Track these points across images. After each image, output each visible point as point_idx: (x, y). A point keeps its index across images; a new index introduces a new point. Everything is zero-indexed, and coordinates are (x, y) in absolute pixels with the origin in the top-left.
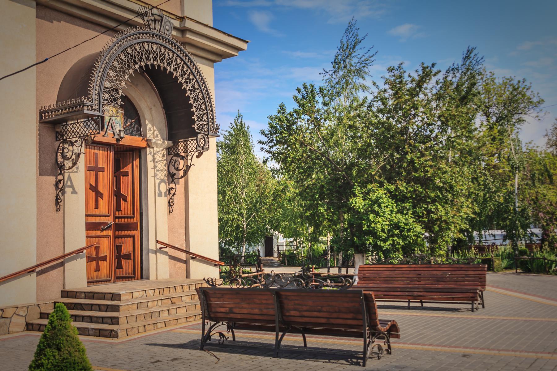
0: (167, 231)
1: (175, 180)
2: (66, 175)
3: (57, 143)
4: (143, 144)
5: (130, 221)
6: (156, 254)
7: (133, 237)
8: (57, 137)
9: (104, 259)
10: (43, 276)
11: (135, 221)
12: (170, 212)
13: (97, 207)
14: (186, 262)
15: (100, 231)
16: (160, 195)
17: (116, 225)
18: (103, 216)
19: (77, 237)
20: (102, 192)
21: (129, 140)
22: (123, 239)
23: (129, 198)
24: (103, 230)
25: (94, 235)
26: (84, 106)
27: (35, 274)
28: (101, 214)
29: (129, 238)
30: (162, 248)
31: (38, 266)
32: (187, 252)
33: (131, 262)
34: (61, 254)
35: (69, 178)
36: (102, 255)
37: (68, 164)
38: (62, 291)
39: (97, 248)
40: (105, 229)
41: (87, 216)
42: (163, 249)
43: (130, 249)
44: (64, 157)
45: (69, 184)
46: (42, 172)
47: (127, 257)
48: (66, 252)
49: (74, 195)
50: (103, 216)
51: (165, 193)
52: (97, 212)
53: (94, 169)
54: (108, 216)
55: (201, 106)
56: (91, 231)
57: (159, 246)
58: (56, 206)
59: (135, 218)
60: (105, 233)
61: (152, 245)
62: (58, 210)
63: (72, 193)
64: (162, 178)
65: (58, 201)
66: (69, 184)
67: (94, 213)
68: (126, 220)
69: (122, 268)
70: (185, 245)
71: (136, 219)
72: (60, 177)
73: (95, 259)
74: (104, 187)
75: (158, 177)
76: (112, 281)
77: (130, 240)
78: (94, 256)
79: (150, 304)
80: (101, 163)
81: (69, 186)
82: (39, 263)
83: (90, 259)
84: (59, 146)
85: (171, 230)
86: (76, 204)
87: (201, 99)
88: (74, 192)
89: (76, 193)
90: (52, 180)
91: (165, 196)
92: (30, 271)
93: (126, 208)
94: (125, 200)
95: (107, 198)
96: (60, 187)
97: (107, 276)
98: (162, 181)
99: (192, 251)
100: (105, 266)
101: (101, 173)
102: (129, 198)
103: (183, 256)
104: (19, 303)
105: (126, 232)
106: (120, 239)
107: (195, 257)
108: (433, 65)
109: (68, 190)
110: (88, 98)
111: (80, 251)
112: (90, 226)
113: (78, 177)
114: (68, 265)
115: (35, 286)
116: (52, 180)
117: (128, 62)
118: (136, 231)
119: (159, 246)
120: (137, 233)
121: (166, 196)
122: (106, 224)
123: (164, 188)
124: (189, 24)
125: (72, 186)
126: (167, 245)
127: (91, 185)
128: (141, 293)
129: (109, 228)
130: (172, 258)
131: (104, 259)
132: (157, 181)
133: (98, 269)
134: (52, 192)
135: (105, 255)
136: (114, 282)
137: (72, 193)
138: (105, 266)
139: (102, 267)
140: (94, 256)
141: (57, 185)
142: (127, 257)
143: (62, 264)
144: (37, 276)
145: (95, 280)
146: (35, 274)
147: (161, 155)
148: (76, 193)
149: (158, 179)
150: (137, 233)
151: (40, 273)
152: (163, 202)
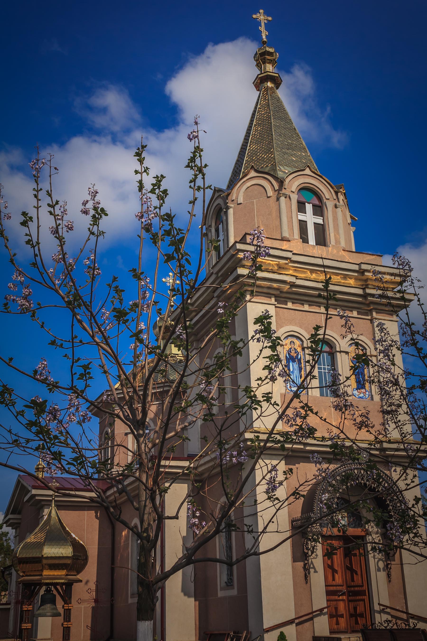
0: (388, 596)
1: (390, 558)
2: (310, 560)
3: (303, 539)
4: (363, 534)
5: (361, 589)
6: (380, 614)
7: (364, 600)
8: (303, 536)
9: (342, 616)
10: (300, 626)
11: (365, 589)
12: (390, 581)
13: (334, 579)
15: (337, 597)
16: (379, 570)
17: (349, 592)
18: (339, 586)
19: (320, 600)
20: (336, 569)
21: (352, 531)
22: (358, 602)
23: (359, 573)
24: (339, 596)
26: (311, 518)
28: (337, 584)
29: (362, 602)
30: (385, 609)
31: (296, 619)
32: (407, 613)
33: (364, 619)
34: (310, 611)
35: (312, 563)
36: (340, 613)
37: (310, 553)
38: (313, 637)
39: (336, 609)
40: (341, 595)
41: (326, 586)
42: (385, 610)
43: (363, 609)
44: (307, 549)
45: (312, 566)
46: (295, 560)
47: (361, 615)
48: (314, 610)
49: (316, 574)
50: (339, 586)
51: (383, 569)
52: (334, 583)
53: (328, 554)
54: (342, 586)
55: (396, 504)
56: (331, 597)
57: (382, 607)
58: (306, 580)
59: (364, 587)
61: (377, 607)
62: (307, 583)
64: (380, 557)
66: (312, 566)
67: (332, 584)
68: (359, 588)
69: (359, 624)
70: (405, 607)
71: (365, 587)
72: (306, 562)
73: (334, 615)
74: (338, 565)
76: (349, 632)
77: (361, 603)
78: (334, 614)
81: (312, 568)
82: (297, 617)
83: (331, 616)
84: (304, 541)
85: (391, 595)
86: (318, 579)
87: (396, 499)
88: (316, 572)
90: (302, 564)
91: (383, 571)
93: (358, 579)
94: (356, 574)
95: (340, 573)
96: (307, 569)
97: (345, 629)
98: (380, 560)
99: (410, 611)
100: (343, 622)
101: (335, 556)
102: (359, 573)
103: (404, 616)
105: (359, 597)
106: (356, 602)
109: (312, 571)
110: (313, 513)
111: (321, 610)
112: (329, 593)
113: (318, 561)
114: (315, 620)
115: (295, 632)
116: (302, 564)
117: (338, 485)
118: (365, 597)
119: (382, 607)
120: (366, 598)
121: (384, 570)
122: (340, 591)
123: (381, 565)
124: (385, 445)
125: (314, 568)
126: (387, 607)
127: (328, 565)
128: (356, 638)
129: (343, 594)
131: (342, 616)
132: (376, 560)
133: (337, 623)
134: (302, 572)
135: (342, 613)
136: (350, 633)
138: (343, 622)
139: (341, 622)
140: (334, 614)
141: (304, 568)
142: (361, 615)
143: (312, 619)
144: (296, 626)
145: (336, 631)
149: (376, 558)
150: (366, 598)
151: (297, 624)
152: (382, 575)
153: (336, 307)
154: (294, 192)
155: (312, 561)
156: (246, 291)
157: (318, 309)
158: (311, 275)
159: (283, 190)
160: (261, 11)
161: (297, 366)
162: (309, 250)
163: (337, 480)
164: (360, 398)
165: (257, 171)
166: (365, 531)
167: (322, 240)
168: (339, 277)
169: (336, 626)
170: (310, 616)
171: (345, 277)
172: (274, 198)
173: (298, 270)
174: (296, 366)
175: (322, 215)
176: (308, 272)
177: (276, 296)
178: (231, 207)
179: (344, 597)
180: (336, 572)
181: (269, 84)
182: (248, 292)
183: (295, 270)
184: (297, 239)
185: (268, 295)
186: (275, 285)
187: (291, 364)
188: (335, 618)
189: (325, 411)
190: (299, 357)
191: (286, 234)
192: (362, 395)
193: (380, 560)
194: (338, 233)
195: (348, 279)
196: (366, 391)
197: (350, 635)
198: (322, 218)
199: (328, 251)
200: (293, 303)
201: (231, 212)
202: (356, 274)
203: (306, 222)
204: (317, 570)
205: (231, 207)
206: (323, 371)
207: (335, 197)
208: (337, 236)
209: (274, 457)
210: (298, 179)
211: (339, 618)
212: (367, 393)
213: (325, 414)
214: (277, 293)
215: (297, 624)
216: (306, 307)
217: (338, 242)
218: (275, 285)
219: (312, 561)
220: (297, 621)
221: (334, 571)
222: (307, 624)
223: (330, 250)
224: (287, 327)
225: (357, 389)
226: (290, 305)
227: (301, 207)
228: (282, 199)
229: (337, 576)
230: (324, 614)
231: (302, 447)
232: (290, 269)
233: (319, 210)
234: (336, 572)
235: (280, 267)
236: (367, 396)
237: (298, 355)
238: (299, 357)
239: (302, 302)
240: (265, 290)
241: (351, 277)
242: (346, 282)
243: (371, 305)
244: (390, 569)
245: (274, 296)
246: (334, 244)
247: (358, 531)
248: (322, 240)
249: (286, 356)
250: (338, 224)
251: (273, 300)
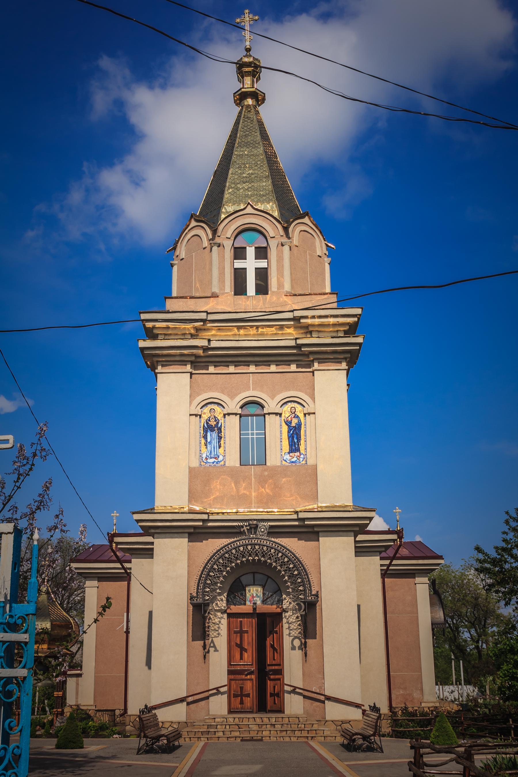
4: (279, 610)
9: (248, 695)
13: (241, 658)
14: (323, 702)
16: (293, 648)
24: (247, 675)
25: (238, 678)
27: (185, 703)
49: (216, 653)
51: (299, 647)
60: (249, 677)
63: (214, 651)
64: (296, 635)
65: (205, 657)
66: (212, 645)
74: (248, 643)
75: (291, 635)
79: (218, 727)
80: (246, 626)
81: (212, 647)
88: (216, 650)
89: (218, 651)
92: (181, 700)
98: (296, 637)
101: (246, 634)
104: (174, 720)
107: (329, 698)
108: (507, 513)
113: (220, 638)
114: (211, 699)
116: (202, 643)
123: (297, 643)
125: (214, 646)
128: (222, 719)
129: (251, 673)
130: (305, 697)
131: (248, 695)
137: (214, 651)
139: (246, 701)
141: (204, 647)
143: (207, 698)
146: (185, 703)
147: (295, 618)
148: (218, 651)
153: (269, 363)
154: (229, 238)
155: (212, 640)
156: (158, 362)
157: (247, 369)
158: (238, 331)
159: (217, 238)
160: (247, 11)
161: (216, 435)
162: (241, 302)
164: (293, 462)
165: (197, 221)
166: (281, 608)
167: (262, 288)
168: (273, 329)
169: (239, 706)
170: (206, 694)
171: (282, 327)
172: (208, 249)
173: (222, 329)
174: (215, 434)
175: (266, 258)
176: (235, 329)
177: (192, 363)
178: (175, 264)
180: (246, 650)
181: (250, 101)
182: (159, 363)
183: (219, 329)
184: (227, 293)
185: (183, 363)
186: (186, 352)
187: (209, 434)
188: (239, 698)
189: (244, 481)
190: (219, 426)
191: (215, 289)
192: (294, 459)
193: (296, 637)
194: (283, 276)
195: (286, 329)
196: (300, 454)
197: (257, 714)
198: (266, 261)
199: (266, 299)
200: (215, 366)
201: (175, 268)
202: (292, 323)
203: (246, 269)
204: (218, 649)
205: (175, 264)
206: (255, 436)
207: (282, 232)
208: (281, 279)
209: (176, 535)
210: (236, 222)
211: (244, 698)
212: (302, 456)
213: (244, 485)
214: (193, 359)
215: (188, 704)
216: (232, 369)
217: (280, 285)
218: (186, 352)
219: (212, 640)
220: (190, 699)
221: (243, 650)
222: (203, 703)
223: (268, 298)
224: (205, 394)
225: (289, 453)
226: (212, 369)
227: (239, 253)
228: (215, 248)
229: (246, 655)
230: (223, 693)
231: (201, 524)
232: (212, 329)
233: (262, 253)
234: (246, 650)
235: (197, 329)
236: (301, 459)
237: (218, 423)
238: (219, 426)
239: (227, 364)
240: (177, 358)
241: (288, 327)
242: (284, 332)
243: (310, 356)
245: (190, 363)
246: (276, 290)
247: (273, 608)
248: (262, 288)
249: (204, 426)
250: (283, 265)
251: (188, 368)
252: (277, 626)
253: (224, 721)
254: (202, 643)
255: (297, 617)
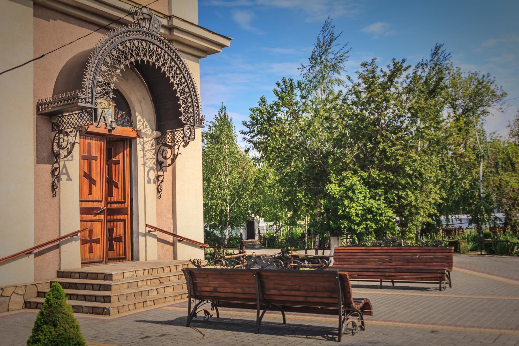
0: (156, 216)
3: (53, 134)
4: (133, 135)
5: (121, 206)
6: (145, 237)
7: (124, 221)
8: (53, 128)
9: (97, 241)
10: (40, 257)
11: (126, 206)
12: (159, 197)
13: (90, 193)
14: (173, 244)
15: (93, 216)
16: (149, 182)
17: (108, 209)
18: (96, 201)
19: (71, 221)
20: (95, 179)
21: (120, 131)
22: (115, 223)
23: (120, 185)
24: (96, 215)
25: (87, 219)
26: (78, 99)
27: (32, 256)
28: (94, 199)
31: (35, 248)
32: (174, 235)
33: (122, 244)
34: (57, 237)
35: (65, 166)
36: (95, 238)
38: (58, 272)
39: (91, 232)
40: (98, 214)
41: (81, 201)
42: (152, 232)
43: (121, 232)
44: (60, 147)
45: (64, 171)
46: (39, 160)
47: (119, 239)
48: (62, 235)
49: (69, 182)
50: (96, 201)
51: (154, 180)
52: (90, 198)
53: (87, 158)
54: (101, 202)
56: (85, 216)
57: (148, 229)
58: (53, 192)
59: (126, 204)
60: (98, 217)
61: (142, 229)
62: (54, 196)
63: (67, 180)
64: (151, 166)
65: (54, 187)
66: (64, 171)
67: (88, 199)
68: (118, 205)
69: (114, 250)
71: (127, 205)
72: (56, 165)
73: (88, 241)
74: (97, 174)
76: (104, 262)
77: (121, 224)
78: (88, 238)
79: (140, 284)
80: (94, 152)
81: (64, 174)
82: (36, 245)
83: (84, 242)
84: (55, 136)
85: (159, 214)
86: (71, 190)
88: (69, 179)
89: (71, 180)
91: (154, 183)
92: (28, 253)
93: (118, 194)
94: (117, 187)
95: (99, 185)
96: (56, 175)
98: (151, 168)
99: (178, 234)
100: (98, 248)
101: (94, 161)
102: (120, 185)
103: (171, 239)
104: (18, 283)
105: (118, 216)
106: (112, 223)
107: (182, 240)
108: (404, 61)
109: (64, 177)
110: (82, 92)
111: (75, 234)
112: (84, 211)
113: (73, 165)
114: (63, 248)
115: (33, 267)
116: (48, 167)
117: (120, 58)
118: (126, 216)
119: (148, 229)
120: (127, 217)
121: (155, 183)
122: (99, 209)
123: (152, 175)
125: (67, 174)
126: (156, 229)
127: (85, 172)
128: (131, 273)
129: (102, 212)
130: (160, 240)
131: (97, 241)
132: (147, 169)
133: (91, 251)
134: (49, 179)
135: (98, 237)
136: (107, 263)
137: (67, 180)
138: (98, 248)
139: (95, 249)
140: (88, 238)
141: (53, 172)
142: (119, 239)
143: (58, 246)
144: (35, 257)
145: (89, 261)
146: (32, 256)
147: (150, 145)
148: (71, 180)
149: (147, 167)
150: (127, 217)
151: (37, 255)
152: (152, 188)
163: (120, 50)
179: (102, 217)
244: (161, 183)
252: (117, 154)
253: (133, 275)
254: (48, 167)
255: (152, 145)
